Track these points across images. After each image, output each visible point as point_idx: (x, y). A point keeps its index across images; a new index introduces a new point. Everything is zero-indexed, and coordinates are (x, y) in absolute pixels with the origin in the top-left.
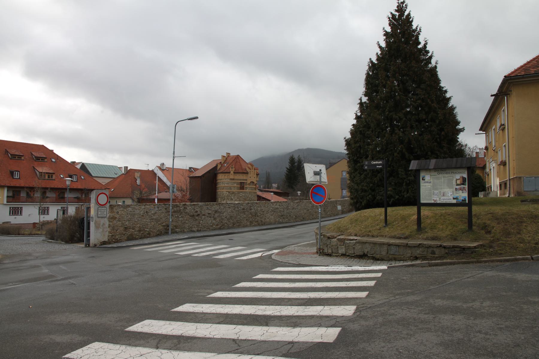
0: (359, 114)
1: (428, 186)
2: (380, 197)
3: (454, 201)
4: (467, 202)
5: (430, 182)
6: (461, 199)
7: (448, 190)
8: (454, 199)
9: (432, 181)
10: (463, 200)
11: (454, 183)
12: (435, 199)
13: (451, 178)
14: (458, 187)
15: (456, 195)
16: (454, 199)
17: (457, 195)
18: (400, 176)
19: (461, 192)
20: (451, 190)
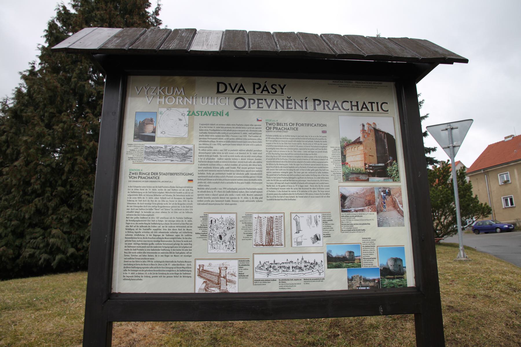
0: (25, 91)
1: (175, 175)
2: (31, 251)
3: (336, 281)
4: (410, 281)
5: (185, 156)
6: (375, 261)
7: (298, 204)
8: (334, 262)
9: (195, 143)
10: (385, 272)
11: (333, 164)
12: (214, 266)
13: (316, 132)
14: (353, 188)
15: (341, 243)
16: (334, 262)
17: (354, 238)
18: (83, 205)
19: (372, 216)
20: (317, 205)
